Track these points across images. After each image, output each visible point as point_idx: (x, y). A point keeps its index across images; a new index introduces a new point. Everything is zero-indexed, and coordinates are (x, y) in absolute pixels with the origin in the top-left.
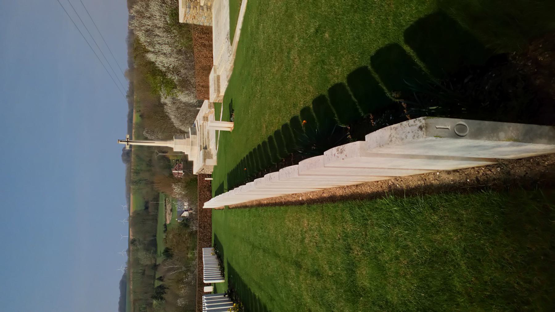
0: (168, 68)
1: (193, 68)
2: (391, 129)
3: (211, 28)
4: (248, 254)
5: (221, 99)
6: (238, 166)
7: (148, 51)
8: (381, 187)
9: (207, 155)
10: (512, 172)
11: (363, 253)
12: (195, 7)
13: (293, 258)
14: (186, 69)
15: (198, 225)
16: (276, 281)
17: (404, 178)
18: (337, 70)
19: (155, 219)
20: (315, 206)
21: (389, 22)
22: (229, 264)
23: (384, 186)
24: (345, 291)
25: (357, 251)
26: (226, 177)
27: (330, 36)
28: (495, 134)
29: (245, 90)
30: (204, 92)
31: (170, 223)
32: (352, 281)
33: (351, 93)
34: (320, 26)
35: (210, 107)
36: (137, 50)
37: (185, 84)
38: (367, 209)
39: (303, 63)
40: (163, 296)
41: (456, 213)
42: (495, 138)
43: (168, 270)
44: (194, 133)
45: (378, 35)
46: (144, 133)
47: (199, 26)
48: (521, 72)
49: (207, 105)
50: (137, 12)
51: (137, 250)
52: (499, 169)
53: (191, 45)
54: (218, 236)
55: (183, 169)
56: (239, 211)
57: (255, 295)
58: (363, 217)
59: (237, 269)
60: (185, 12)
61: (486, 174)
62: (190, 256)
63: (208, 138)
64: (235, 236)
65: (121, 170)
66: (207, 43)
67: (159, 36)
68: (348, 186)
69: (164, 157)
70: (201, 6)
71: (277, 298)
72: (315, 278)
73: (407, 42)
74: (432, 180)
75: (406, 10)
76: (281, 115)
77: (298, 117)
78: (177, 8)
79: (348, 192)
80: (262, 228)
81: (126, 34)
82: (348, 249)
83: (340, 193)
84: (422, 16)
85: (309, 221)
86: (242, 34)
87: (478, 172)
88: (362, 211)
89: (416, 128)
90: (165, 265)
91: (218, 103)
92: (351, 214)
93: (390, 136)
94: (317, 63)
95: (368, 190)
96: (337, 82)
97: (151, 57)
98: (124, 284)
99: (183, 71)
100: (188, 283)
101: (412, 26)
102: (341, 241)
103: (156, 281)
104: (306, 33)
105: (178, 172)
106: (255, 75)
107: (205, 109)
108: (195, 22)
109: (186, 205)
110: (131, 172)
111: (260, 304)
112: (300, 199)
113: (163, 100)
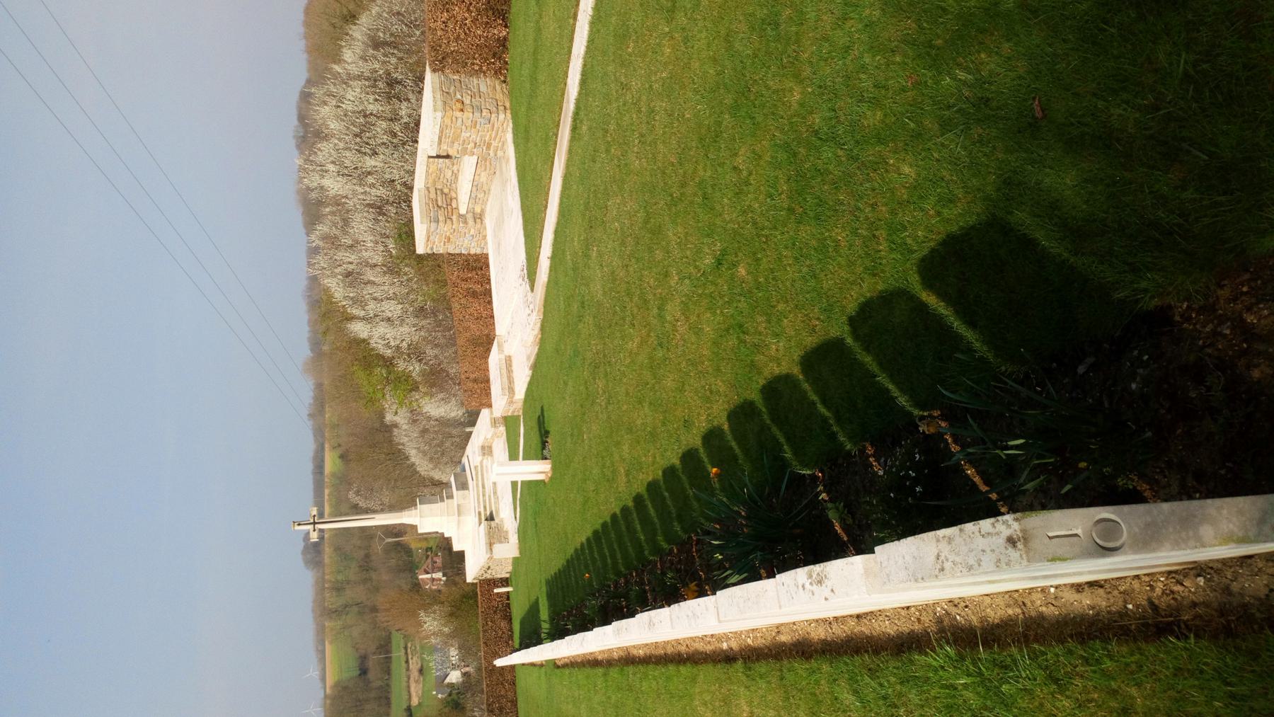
1: (452, 341)
2: (938, 541)
3: (486, 257)
6: (570, 563)
7: (352, 318)
8: (919, 620)
9: (495, 537)
10: (1235, 587)
14: (437, 346)
15: (484, 707)
17: (971, 599)
18: (776, 346)
19: (385, 698)
20: (762, 667)
23: (926, 619)
26: (544, 589)
28: (1191, 533)
29: (570, 389)
30: (479, 392)
31: (420, 704)
33: (814, 397)
34: (724, 252)
35: (494, 422)
36: (328, 316)
37: (437, 379)
38: (893, 679)
41: (1114, 693)
42: (1192, 543)
44: (463, 486)
47: (460, 255)
48: (1209, 351)
49: (488, 420)
50: (325, 238)
52: (1201, 581)
53: (444, 296)
55: (443, 569)
56: (580, 675)
58: (885, 698)
60: (428, 231)
61: (1172, 592)
63: (495, 493)
65: (301, 586)
66: (478, 288)
67: (373, 283)
68: (836, 618)
69: (398, 544)
70: (460, 216)
74: (1038, 605)
75: (914, 217)
77: (697, 450)
79: (839, 631)
81: (303, 284)
83: (819, 634)
84: (954, 229)
86: (553, 268)
87: (1151, 586)
88: (881, 685)
89: (1001, 541)
92: (855, 692)
93: (938, 557)
95: (888, 628)
96: (777, 371)
97: (359, 329)
99: (430, 352)
101: (933, 251)
104: (696, 267)
105: (431, 578)
106: (589, 355)
107: (485, 430)
108: (452, 249)
110: (323, 578)
112: (725, 646)
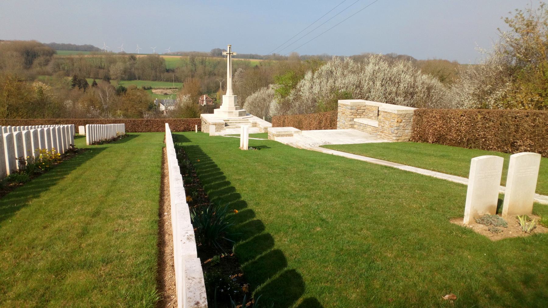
0: (300, 91)
1: (301, 113)
3: (336, 129)
4: (113, 167)
5: (271, 138)
7: (313, 73)
9: (219, 127)
11: (102, 276)
12: (352, 114)
13: (103, 209)
14: (300, 106)
15: (149, 119)
16: (81, 194)
21: (325, 283)
22: (104, 149)
23: (170, 292)
24: (63, 261)
25: (104, 270)
27: (317, 232)
30: (279, 122)
31: (152, 93)
32: (72, 267)
34: (328, 222)
35: (266, 129)
36: (314, 63)
37: (286, 106)
39: (295, 210)
40: (77, 87)
43: (103, 92)
44: (241, 114)
45: (315, 275)
46: (240, 69)
50: (348, 63)
51: (125, 62)
53: (320, 111)
54: (137, 138)
56: (159, 156)
57: (68, 174)
58: (140, 273)
59: (98, 156)
60: (347, 105)
62: (119, 112)
63: (237, 127)
64: (133, 153)
65: (204, 46)
66: (323, 124)
69: (219, 87)
70: (353, 119)
71: (62, 196)
72: (80, 231)
73: (306, 301)
76: (250, 192)
77: (246, 207)
78: (351, 98)
79: (168, 258)
80: (138, 178)
81: (330, 54)
82: (107, 261)
83: (167, 250)
85: (143, 222)
88: (145, 272)
89: (198, 300)
90: (109, 88)
91: (267, 136)
93: (194, 278)
94: (294, 222)
96: (276, 240)
97: (308, 75)
98: (90, 49)
99: (297, 104)
100: (88, 111)
101: (319, 303)
102: (116, 254)
103: (92, 80)
105: (204, 100)
107: (263, 124)
108: (339, 114)
109: (172, 108)
111: (59, 179)
112: (166, 214)
113: (271, 86)
